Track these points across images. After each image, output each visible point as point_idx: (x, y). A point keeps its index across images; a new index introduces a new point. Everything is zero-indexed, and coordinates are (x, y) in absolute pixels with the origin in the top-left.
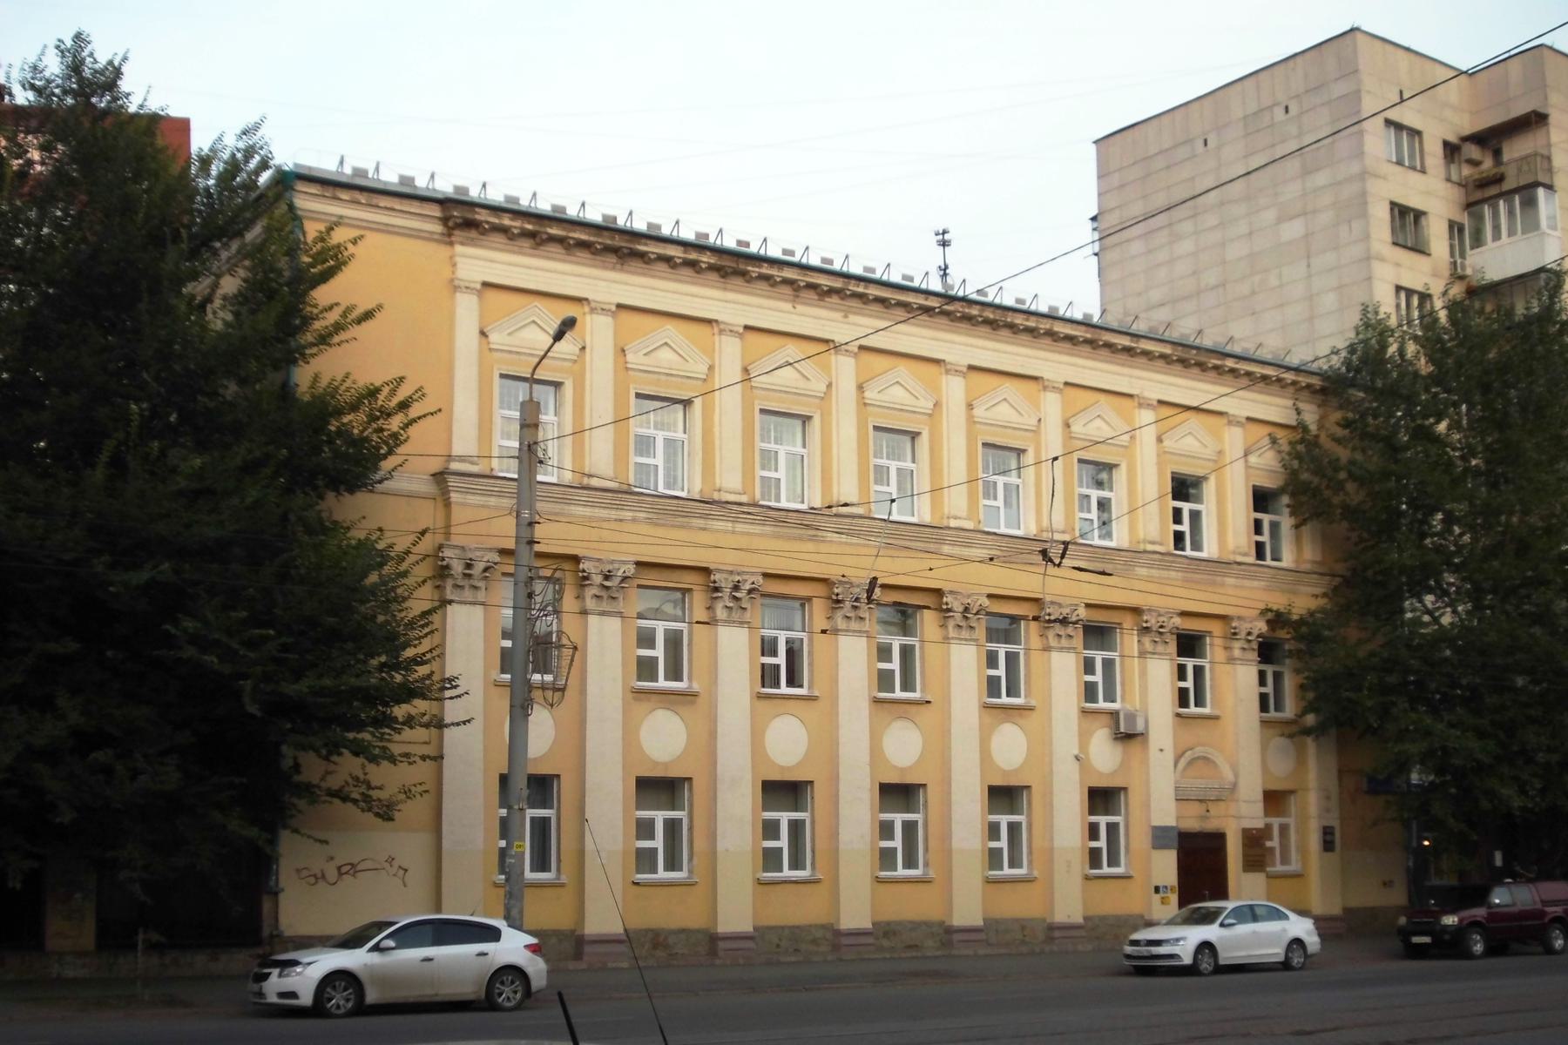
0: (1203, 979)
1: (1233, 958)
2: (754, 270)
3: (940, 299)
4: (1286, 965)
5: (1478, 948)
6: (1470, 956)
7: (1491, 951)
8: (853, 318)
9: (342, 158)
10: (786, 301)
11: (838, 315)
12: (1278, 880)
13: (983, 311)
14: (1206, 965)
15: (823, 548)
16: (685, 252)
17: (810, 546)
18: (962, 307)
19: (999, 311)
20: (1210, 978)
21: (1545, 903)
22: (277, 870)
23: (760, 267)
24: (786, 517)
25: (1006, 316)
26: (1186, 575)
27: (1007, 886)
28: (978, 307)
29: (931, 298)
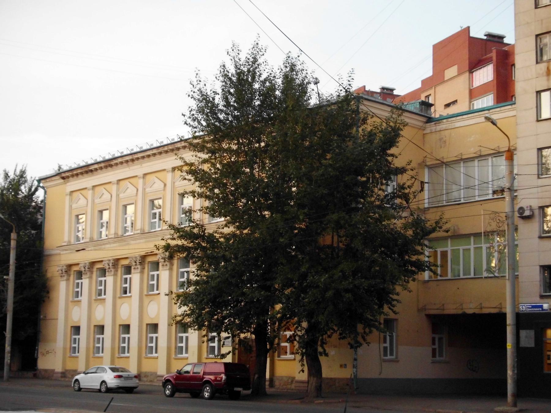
0: (204, 400)
1: (85, 386)
2: (112, 163)
3: (390, 108)
4: (100, 391)
5: (206, 395)
6: (203, 397)
7: (211, 398)
8: (144, 165)
9: (456, 101)
10: (126, 168)
11: (139, 166)
12: (283, 361)
13: (168, 147)
14: (103, 389)
15: (131, 247)
16: (98, 165)
17: (127, 247)
18: (162, 149)
19: (172, 145)
20: (103, 394)
21: (205, 373)
22: (38, 349)
23: (113, 161)
24: (109, 241)
25: (175, 146)
26: (146, 240)
27: (180, 360)
28: (166, 147)
29: (154, 150)
